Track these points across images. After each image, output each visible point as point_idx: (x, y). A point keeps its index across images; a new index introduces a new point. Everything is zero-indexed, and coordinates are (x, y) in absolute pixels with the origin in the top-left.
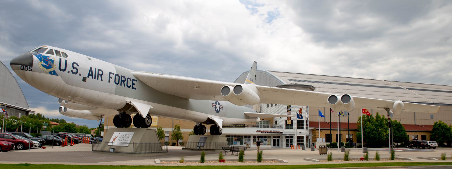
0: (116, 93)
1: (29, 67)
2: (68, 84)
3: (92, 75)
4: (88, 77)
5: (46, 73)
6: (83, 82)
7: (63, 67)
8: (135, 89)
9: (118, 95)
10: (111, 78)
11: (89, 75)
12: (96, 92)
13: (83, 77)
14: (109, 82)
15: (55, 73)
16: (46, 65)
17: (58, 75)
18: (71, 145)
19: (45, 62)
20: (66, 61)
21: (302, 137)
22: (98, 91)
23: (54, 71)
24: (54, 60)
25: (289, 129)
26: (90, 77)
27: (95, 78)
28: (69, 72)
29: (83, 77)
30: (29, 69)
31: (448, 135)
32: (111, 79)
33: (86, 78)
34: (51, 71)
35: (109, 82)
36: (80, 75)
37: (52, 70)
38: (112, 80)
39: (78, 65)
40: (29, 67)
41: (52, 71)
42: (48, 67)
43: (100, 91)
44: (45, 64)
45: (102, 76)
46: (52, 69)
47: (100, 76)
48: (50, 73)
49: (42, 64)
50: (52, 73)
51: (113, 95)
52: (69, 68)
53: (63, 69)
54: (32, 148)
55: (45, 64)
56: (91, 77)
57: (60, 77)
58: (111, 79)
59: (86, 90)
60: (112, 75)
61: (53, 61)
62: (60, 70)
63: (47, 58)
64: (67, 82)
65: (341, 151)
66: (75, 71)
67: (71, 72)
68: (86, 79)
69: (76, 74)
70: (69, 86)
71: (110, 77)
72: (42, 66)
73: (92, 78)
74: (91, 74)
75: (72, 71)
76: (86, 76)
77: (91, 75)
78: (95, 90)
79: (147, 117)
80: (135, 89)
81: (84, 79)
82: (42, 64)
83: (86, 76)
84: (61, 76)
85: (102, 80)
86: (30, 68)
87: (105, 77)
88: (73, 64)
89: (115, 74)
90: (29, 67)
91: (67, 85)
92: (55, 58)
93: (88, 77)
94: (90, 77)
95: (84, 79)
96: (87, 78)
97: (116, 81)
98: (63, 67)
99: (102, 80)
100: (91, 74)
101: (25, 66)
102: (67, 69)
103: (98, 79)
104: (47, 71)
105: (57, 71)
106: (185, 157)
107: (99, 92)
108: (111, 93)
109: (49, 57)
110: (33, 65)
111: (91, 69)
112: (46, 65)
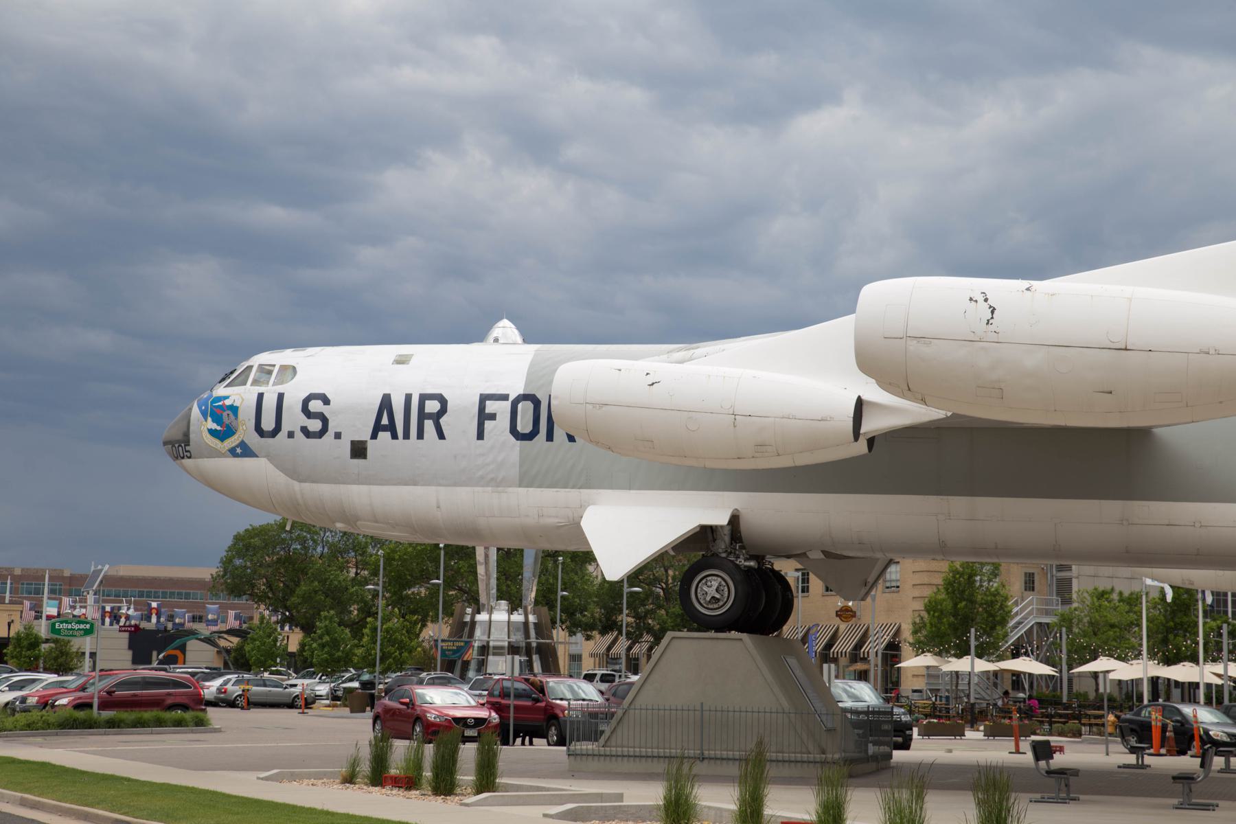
0: (527, 480)
1: (183, 445)
2: (300, 481)
3: (391, 428)
4: (374, 436)
5: (223, 454)
6: (356, 461)
7: (268, 423)
8: (982, 293)
9: (540, 486)
10: (493, 417)
11: (377, 429)
12: (419, 490)
13: (353, 443)
14: (480, 436)
15: (245, 451)
16: (219, 428)
17: (257, 456)
18: (303, 713)
19: (217, 420)
20: (281, 397)
21: (35, 616)
22: (429, 485)
23: (242, 444)
24: (238, 405)
25: (810, 585)
26: (384, 436)
27: (407, 436)
28: (291, 435)
29: (353, 443)
30: (186, 451)
31: (305, 534)
32: (488, 425)
33: (365, 442)
34: (234, 445)
35: (480, 436)
36: (338, 436)
37: (238, 442)
38: (498, 429)
39: (326, 401)
40: (183, 445)
41: (237, 446)
42: (223, 434)
43: (440, 485)
44: (214, 426)
45: (442, 421)
46: (236, 437)
47: (429, 425)
48: (233, 452)
49: (209, 428)
50: (239, 450)
51: (510, 489)
52: (294, 418)
53: (271, 430)
54: (378, 722)
55: (214, 426)
56: (388, 434)
57: (262, 459)
58: (488, 425)
59: (376, 489)
60: (491, 406)
61: (234, 409)
62: (259, 437)
63: (220, 403)
64: (293, 473)
65: (919, 732)
66: (315, 425)
67: (299, 435)
68: (365, 449)
69: (320, 437)
70: (307, 486)
71: (484, 417)
72: (209, 436)
73: (395, 436)
74: (385, 421)
75: (305, 430)
76: (365, 435)
77: (385, 428)
78: (415, 484)
79: (600, 577)
80: (982, 293)
81: (359, 450)
82: (208, 429)
83: (365, 435)
84: (267, 456)
85: (441, 436)
86: (188, 448)
87: (460, 421)
88: (306, 403)
89: (511, 398)
90: (185, 446)
91: (296, 486)
92: (242, 398)
93: (374, 436)
94: (384, 436)
95: (359, 450)
96: (371, 445)
97: (519, 428)
98: (268, 423)
99: (441, 436)
100: (385, 421)
101: (177, 445)
102: (286, 427)
103: (420, 435)
104: (224, 448)
105: (253, 440)
106: (773, 786)
107: (433, 488)
108: (497, 483)
109: (227, 398)
110: (191, 436)
111: (386, 403)
112: (219, 428)
